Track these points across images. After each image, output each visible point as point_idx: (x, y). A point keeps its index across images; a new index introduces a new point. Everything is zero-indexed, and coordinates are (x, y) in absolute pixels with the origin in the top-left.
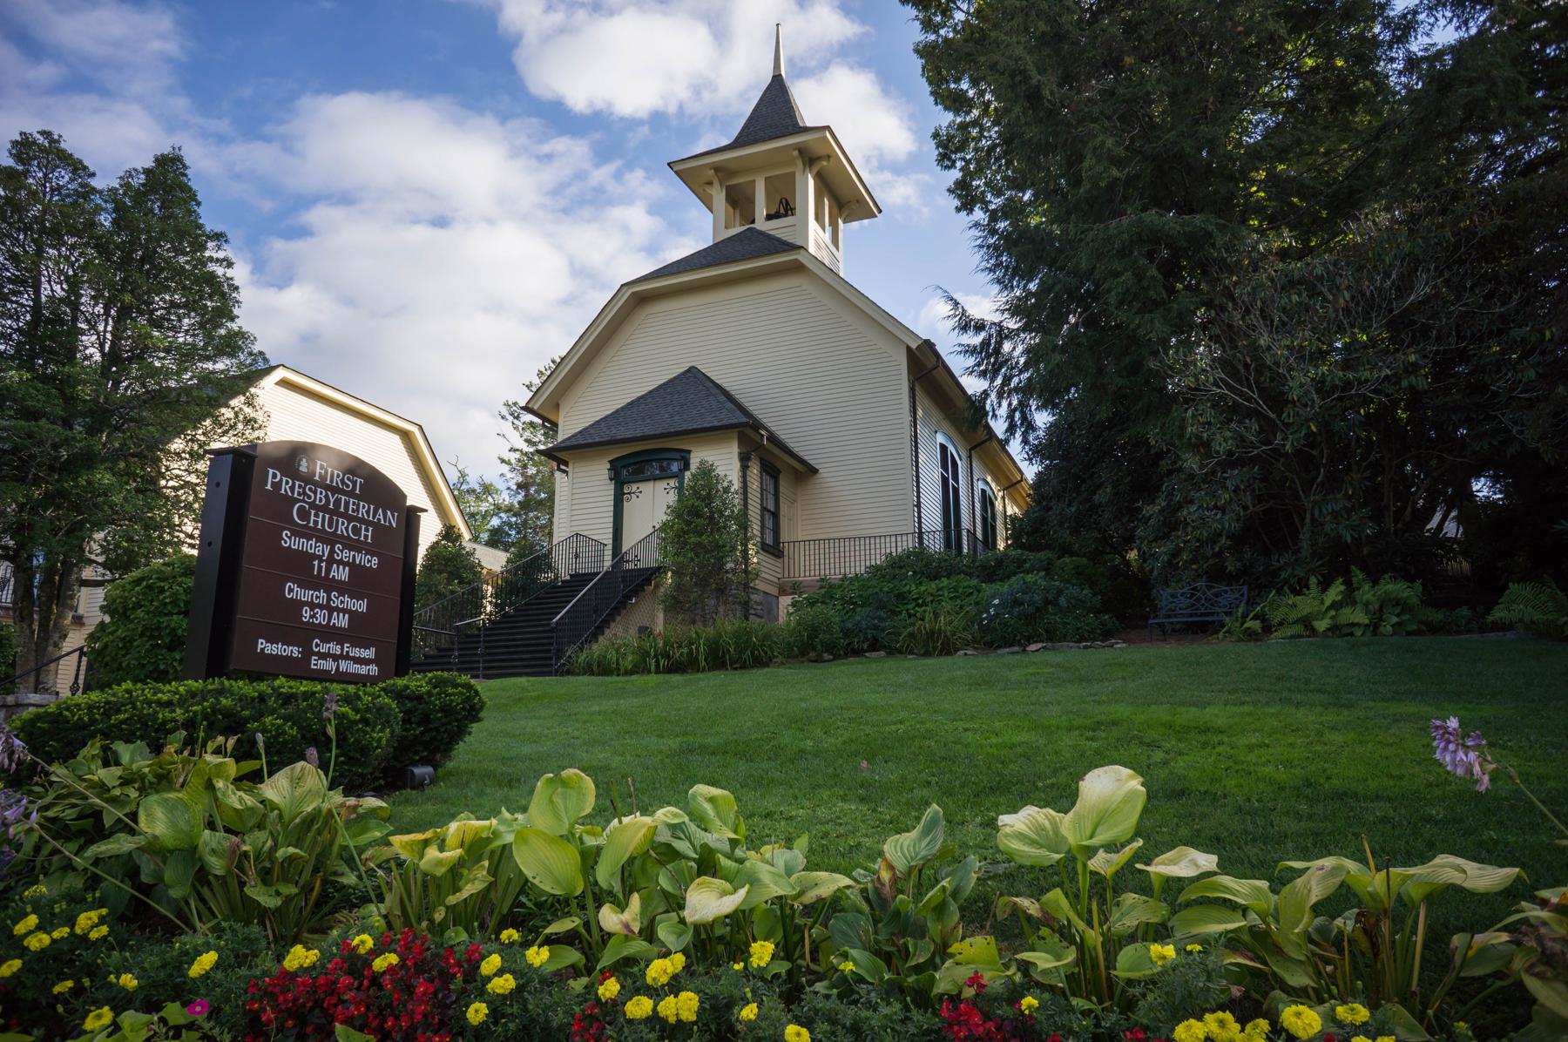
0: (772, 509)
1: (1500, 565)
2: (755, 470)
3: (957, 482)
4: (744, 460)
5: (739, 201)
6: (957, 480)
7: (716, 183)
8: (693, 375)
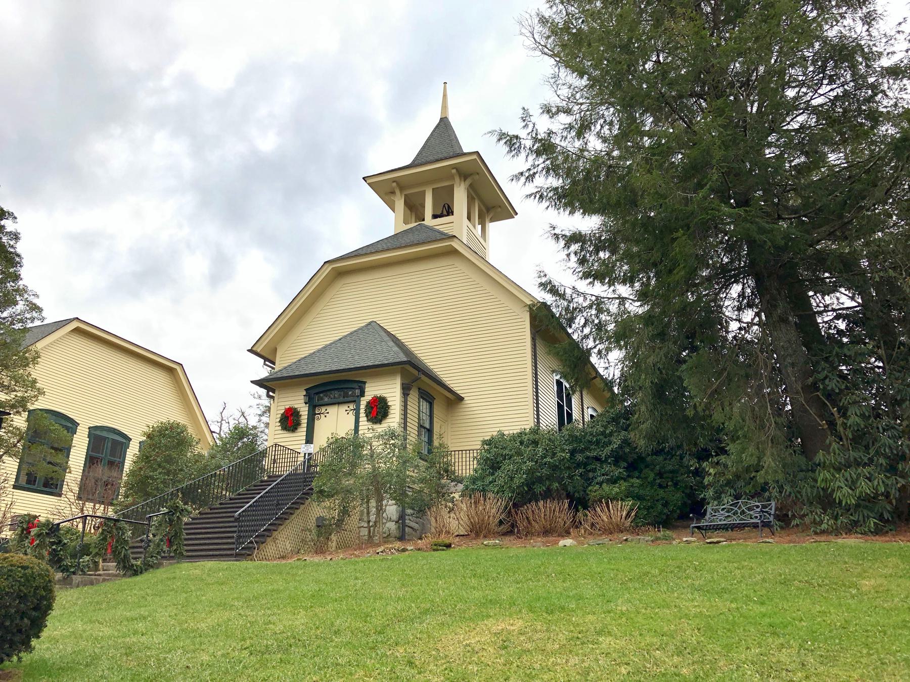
0: (427, 426)
2: (413, 397)
3: (571, 410)
5: (414, 208)
7: (398, 192)
8: (372, 326)
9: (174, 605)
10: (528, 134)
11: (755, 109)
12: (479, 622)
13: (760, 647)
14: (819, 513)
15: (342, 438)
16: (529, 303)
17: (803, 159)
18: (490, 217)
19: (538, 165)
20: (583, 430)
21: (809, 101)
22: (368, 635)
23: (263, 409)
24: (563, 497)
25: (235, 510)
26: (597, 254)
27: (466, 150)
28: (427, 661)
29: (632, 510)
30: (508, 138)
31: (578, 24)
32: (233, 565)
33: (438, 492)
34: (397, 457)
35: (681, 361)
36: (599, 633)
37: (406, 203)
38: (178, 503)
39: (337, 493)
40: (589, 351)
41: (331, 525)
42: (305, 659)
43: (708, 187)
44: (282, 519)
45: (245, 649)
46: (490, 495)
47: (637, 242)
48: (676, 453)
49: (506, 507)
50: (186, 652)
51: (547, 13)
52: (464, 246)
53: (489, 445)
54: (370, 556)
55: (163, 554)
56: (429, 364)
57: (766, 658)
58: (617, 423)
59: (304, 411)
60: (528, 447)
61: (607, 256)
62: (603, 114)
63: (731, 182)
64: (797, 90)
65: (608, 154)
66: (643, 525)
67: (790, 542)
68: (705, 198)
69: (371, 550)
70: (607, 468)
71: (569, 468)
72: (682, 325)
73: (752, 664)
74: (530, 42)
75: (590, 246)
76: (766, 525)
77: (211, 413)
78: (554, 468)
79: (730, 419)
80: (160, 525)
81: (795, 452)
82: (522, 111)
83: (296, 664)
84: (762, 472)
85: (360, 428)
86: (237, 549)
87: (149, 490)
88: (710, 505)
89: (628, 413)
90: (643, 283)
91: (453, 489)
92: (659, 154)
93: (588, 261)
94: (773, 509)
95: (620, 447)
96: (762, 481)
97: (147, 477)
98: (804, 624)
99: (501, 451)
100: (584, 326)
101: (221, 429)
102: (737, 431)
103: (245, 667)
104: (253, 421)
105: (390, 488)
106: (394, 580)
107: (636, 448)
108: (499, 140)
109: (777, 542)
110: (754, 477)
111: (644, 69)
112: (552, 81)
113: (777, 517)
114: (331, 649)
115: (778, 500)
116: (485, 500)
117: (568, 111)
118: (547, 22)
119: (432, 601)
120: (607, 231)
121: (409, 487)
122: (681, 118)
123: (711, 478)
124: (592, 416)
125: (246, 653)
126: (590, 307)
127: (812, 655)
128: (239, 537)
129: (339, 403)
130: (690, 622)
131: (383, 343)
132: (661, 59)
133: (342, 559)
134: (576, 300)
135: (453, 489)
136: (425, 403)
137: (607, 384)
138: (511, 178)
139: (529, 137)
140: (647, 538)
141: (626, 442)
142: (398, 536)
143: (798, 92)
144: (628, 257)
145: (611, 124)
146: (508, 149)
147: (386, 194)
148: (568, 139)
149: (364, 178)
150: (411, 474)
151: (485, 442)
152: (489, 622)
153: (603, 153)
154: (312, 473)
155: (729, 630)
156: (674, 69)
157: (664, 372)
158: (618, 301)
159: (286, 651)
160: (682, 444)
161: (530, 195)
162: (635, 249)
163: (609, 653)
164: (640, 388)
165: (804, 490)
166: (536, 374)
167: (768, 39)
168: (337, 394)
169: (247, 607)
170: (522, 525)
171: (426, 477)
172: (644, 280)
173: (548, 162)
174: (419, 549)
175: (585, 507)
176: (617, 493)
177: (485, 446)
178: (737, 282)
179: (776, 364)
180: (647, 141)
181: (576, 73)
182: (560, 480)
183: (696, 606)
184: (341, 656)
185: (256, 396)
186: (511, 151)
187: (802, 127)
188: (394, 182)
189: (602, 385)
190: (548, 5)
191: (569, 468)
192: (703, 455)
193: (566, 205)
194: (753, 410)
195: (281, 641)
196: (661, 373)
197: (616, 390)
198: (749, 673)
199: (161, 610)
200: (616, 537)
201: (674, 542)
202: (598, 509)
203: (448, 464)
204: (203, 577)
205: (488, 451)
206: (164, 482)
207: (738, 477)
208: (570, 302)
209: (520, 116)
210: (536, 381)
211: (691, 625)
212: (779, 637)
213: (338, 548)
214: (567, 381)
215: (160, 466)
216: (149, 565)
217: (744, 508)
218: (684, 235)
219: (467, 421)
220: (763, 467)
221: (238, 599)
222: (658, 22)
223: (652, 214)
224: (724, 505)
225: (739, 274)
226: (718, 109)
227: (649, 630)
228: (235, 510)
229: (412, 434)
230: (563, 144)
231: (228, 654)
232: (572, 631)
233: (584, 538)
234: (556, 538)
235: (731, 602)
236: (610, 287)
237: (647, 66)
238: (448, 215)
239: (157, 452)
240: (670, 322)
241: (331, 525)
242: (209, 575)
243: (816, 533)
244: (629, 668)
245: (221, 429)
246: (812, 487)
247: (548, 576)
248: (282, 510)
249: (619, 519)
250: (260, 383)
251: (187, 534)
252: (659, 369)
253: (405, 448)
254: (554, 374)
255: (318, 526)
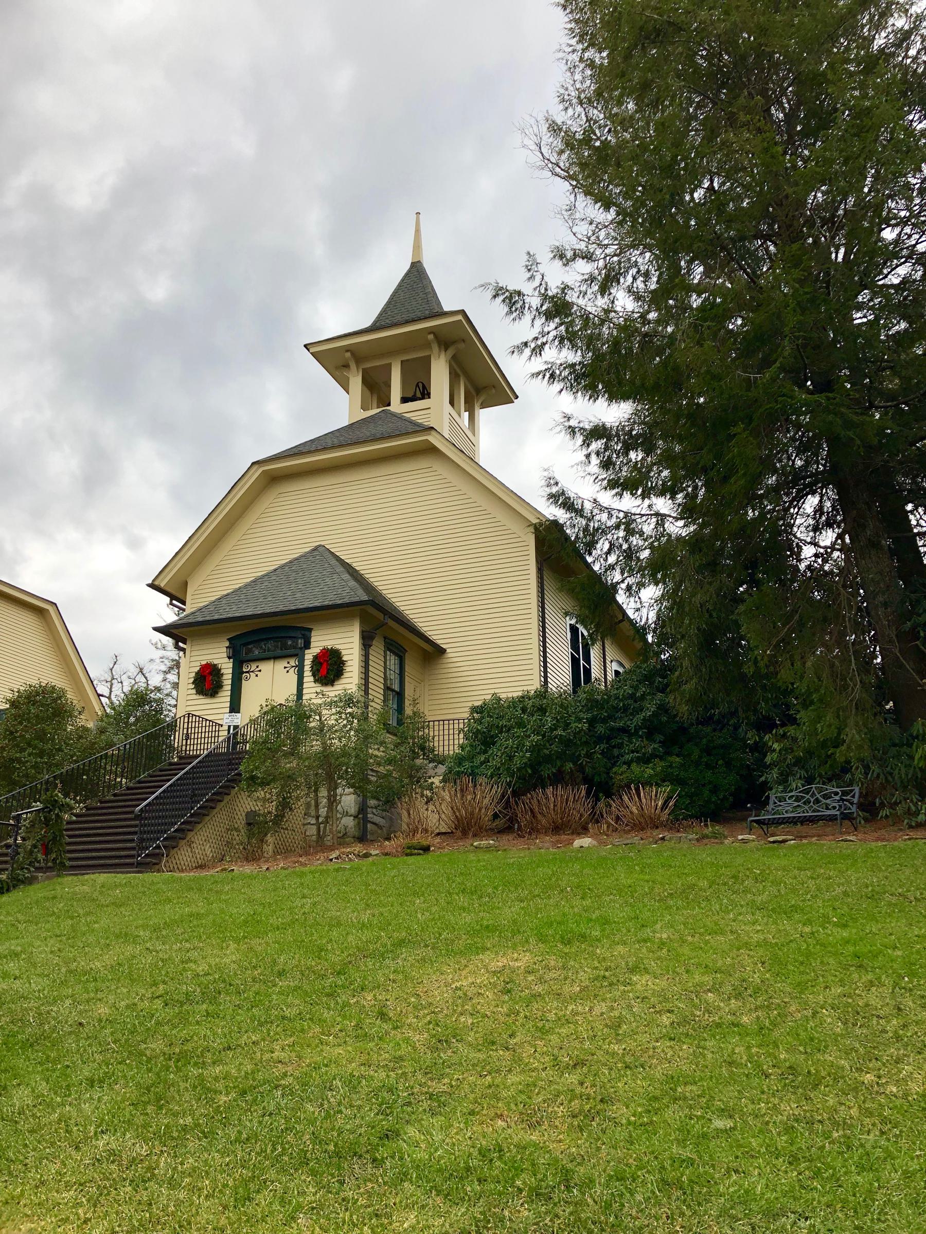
1: (903, 325)
3: (589, 664)
4: (366, 641)
6: (588, 661)
7: (353, 365)
9: (57, 936)
10: (535, 289)
11: (840, 258)
12: (472, 957)
13: (843, 986)
14: (915, 800)
15: (281, 705)
16: (535, 521)
17: (903, 325)
18: (480, 401)
19: (549, 333)
20: (606, 692)
21: (914, 246)
22: (323, 977)
23: (169, 664)
24: (578, 781)
25: (134, 803)
26: (627, 455)
27: (446, 308)
28: (404, 1011)
29: (669, 798)
30: (507, 294)
31: (605, 135)
32: (135, 878)
33: (411, 777)
34: (356, 731)
35: (738, 600)
36: (633, 970)
37: (365, 382)
38: (57, 795)
39: (274, 780)
40: (614, 588)
41: (266, 823)
42: (240, 1011)
43: (778, 364)
44: (200, 816)
45: (158, 997)
46: (482, 780)
47: (681, 440)
48: (728, 721)
49: (503, 796)
50: (76, 1002)
51: (560, 118)
52: (445, 442)
53: (481, 713)
54: (321, 865)
55: (37, 865)
56: (398, 604)
57: (850, 1001)
58: (651, 683)
59: (227, 668)
60: (533, 715)
61: (639, 458)
62: (636, 261)
63: (807, 358)
64: (897, 230)
65: (643, 316)
66: (685, 818)
67: (878, 839)
68: (773, 380)
69: (322, 856)
70: (636, 742)
71: (586, 743)
72: (739, 551)
73: (833, 1008)
74: (536, 158)
75: (617, 443)
76: (847, 817)
77: (97, 670)
78: (567, 743)
79: (802, 677)
80: (33, 826)
81: (886, 720)
82: (527, 257)
83: (228, 1017)
84: (844, 748)
85: (305, 691)
86: (139, 856)
87: (15, 776)
88: (774, 791)
89: (666, 669)
90: (687, 494)
91: (431, 772)
92: (712, 320)
93: (614, 464)
94: (857, 796)
95: (655, 714)
96: (843, 759)
97: (12, 760)
98: (899, 953)
99: (496, 722)
100: (609, 552)
101: (111, 691)
102: (810, 694)
103: (158, 1023)
104: (155, 680)
105: (346, 771)
106: (355, 899)
107: (676, 716)
108: (495, 297)
109: (860, 840)
110: (832, 754)
111: (692, 199)
112: (566, 214)
113: (861, 806)
114: (274, 997)
115: (862, 784)
116: (475, 786)
117: (588, 257)
118: (560, 130)
119: (408, 928)
120: (639, 424)
121: (372, 770)
122: (742, 268)
123: (775, 756)
124: (617, 673)
125: (159, 1003)
126: (617, 527)
127: (911, 995)
128: (142, 840)
129: (276, 658)
130: (752, 953)
131: (335, 576)
132: (716, 185)
133: (282, 868)
134: (597, 518)
135: (431, 772)
136: (393, 657)
137: (639, 631)
138: (512, 349)
139: (537, 293)
140: (690, 837)
141: (663, 708)
142: (357, 834)
143: (899, 235)
144: (667, 460)
145: (647, 275)
146: (506, 309)
147: (337, 368)
148: (589, 296)
149: (305, 346)
150: (376, 753)
151: (474, 710)
152: (486, 957)
153: (636, 315)
154: (240, 753)
155: (802, 963)
156: (732, 200)
157: (714, 615)
158: (654, 520)
159: (214, 1001)
160: (736, 711)
161: (538, 374)
162: (677, 448)
163: (646, 997)
164: (683, 637)
165: (897, 771)
166: (543, 617)
167: (861, 160)
168: (271, 644)
169: (158, 938)
170: (524, 820)
171: (395, 757)
172: (690, 489)
173: (563, 328)
174: (387, 854)
175: (609, 795)
176: (651, 776)
177: (475, 715)
178: (813, 493)
179: (863, 603)
180: (696, 301)
181: (599, 204)
182: (575, 759)
183: (758, 931)
184: (288, 1006)
185: (159, 645)
186: (511, 312)
187: (905, 281)
188: (347, 351)
189: (632, 632)
190: (561, 107)
191: (586, 743)
192: (765, 725)
193: (586, 388)
194: (832, 666)
195: (207, 987)
196: (711, 616)
197: (650, 638)
198: (829, 1020)
199: (39, 943)
200: (649, 834)
201: (726, 841)
202: (625, 798)
203: (425, 739)
204: (94, 896)
205: (479, 721)
206: (35, 766)
207: (810, 753)
208: (589, 520)
209: (524, 264)
210: (544, 627)
211: (753, 957)
212: (867, 971)
213: (276, 853)
214: (586, 627)
215: (29, 745)
216: (19, 880)
217: (818, 796)
218: (744, 430)
219: (452, 680)
220: (844, 741)
221: (144, 927)
222: (711, 133)
223: (702, 400)
224: (791, 791)
225: (815, 483)
226: (793, 256)
227: (698, 965)
228: (134, 803)
229: (376, 700)
230: (581, 302)
231: (135, 1004)
232: (596, 968)
233: (607, 835)
234: (570, 837)
235: (804, 924)
236: (643, 499)
237: (696, 195)
238: (423, 398)
239: (26, 726)
240: (722, 548)
241: (266, 823)
242: (101, 893)
243: (911, 827)
244: (673, 1017)
245: (111, 691)
246: (908, 766)
247: (562, 891)
248: (199, 802)
249: (653, 811)
250: (164, 630)
251: (70, 837)
252: (708, 611)
253: (366, 718)
254: (568, 618)
255: (249, 824)
